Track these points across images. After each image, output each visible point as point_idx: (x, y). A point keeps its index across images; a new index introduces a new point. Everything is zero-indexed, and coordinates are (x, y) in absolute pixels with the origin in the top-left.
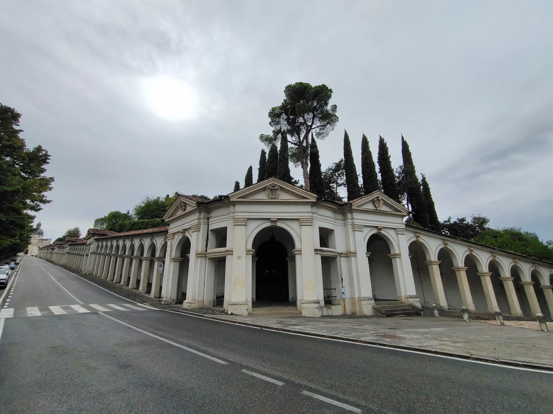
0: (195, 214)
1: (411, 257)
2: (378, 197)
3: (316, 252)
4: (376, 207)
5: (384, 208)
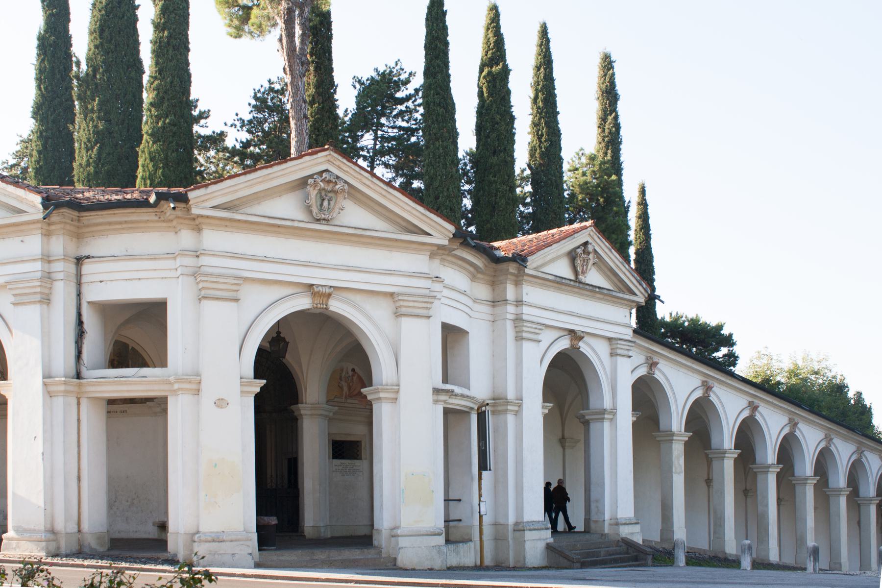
0: (26, 239)
2: (586, 244)
3: (435, 398)
4: (576, 273)
5: (594, 277)
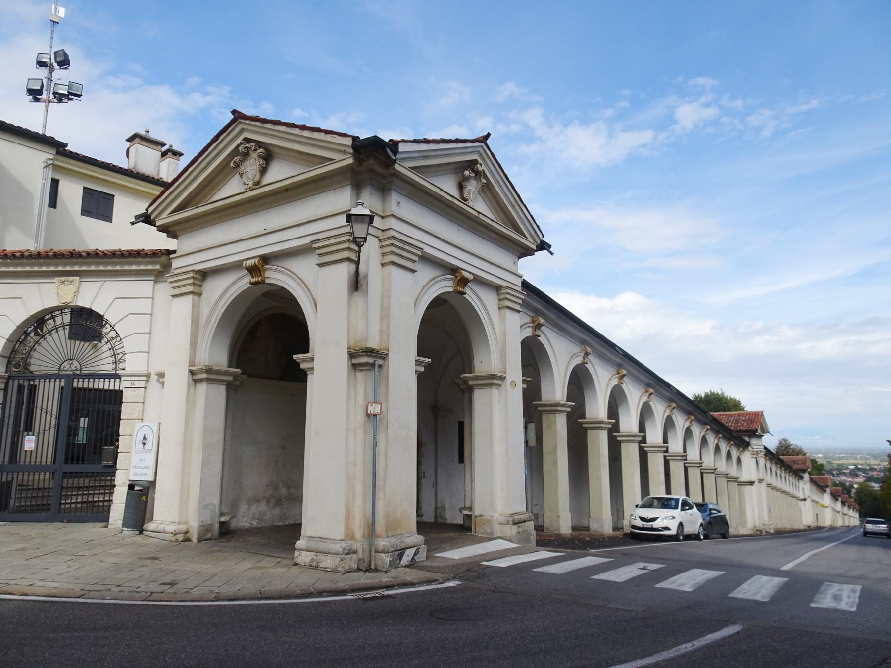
1: (422, 369)
